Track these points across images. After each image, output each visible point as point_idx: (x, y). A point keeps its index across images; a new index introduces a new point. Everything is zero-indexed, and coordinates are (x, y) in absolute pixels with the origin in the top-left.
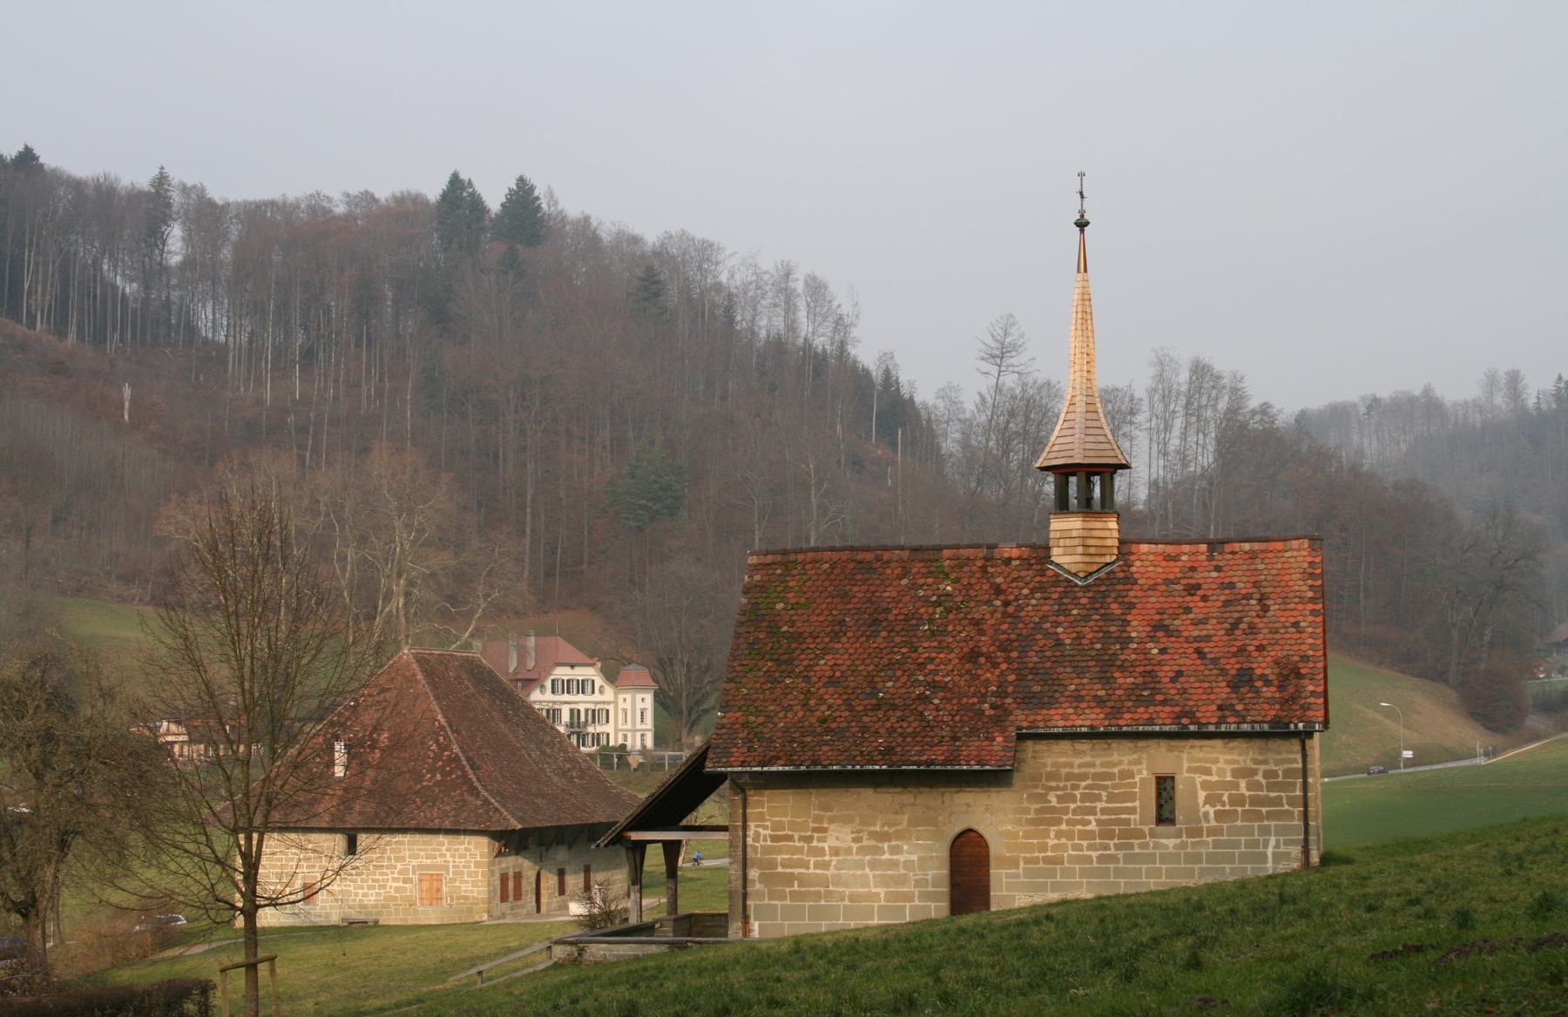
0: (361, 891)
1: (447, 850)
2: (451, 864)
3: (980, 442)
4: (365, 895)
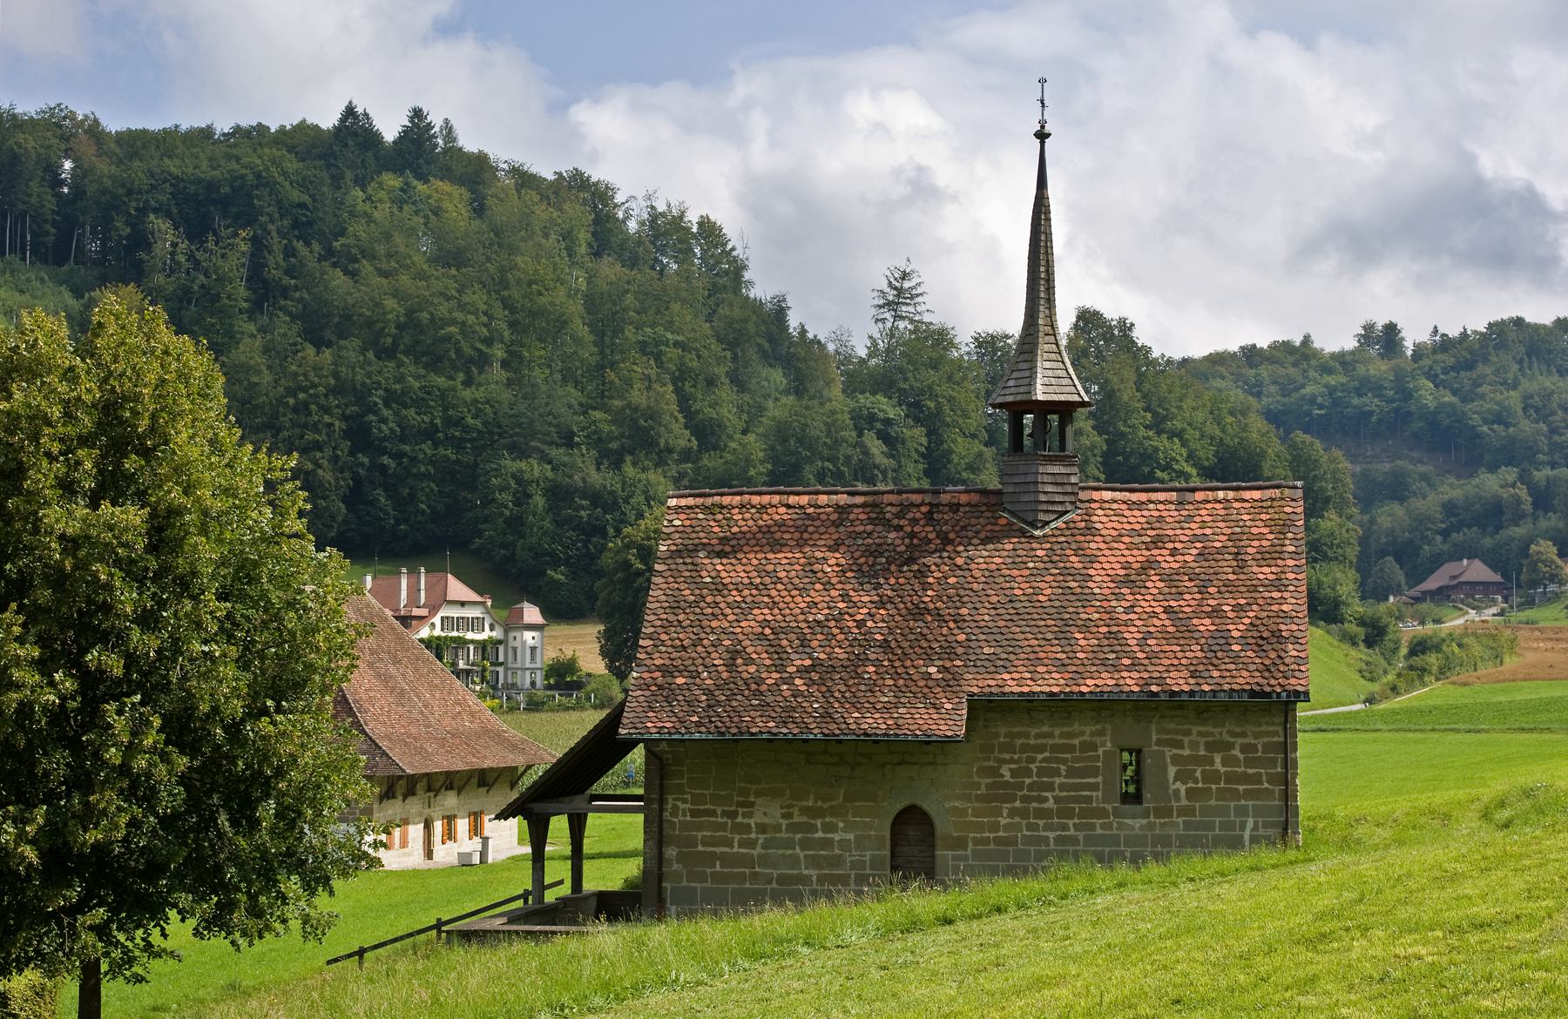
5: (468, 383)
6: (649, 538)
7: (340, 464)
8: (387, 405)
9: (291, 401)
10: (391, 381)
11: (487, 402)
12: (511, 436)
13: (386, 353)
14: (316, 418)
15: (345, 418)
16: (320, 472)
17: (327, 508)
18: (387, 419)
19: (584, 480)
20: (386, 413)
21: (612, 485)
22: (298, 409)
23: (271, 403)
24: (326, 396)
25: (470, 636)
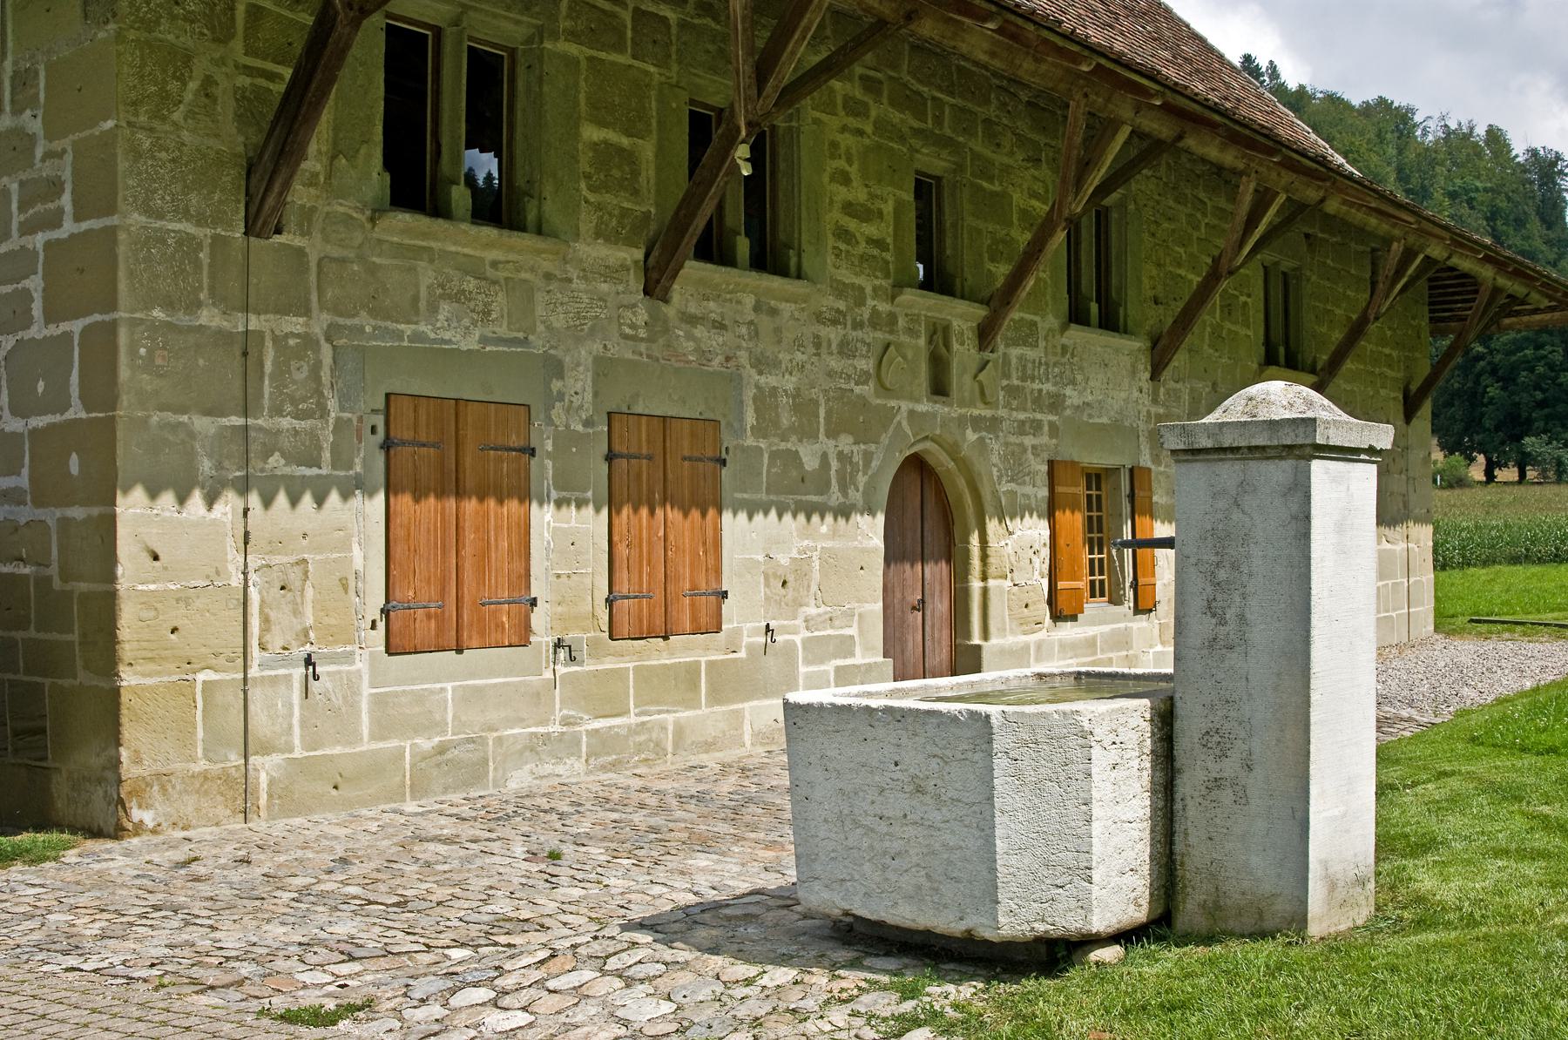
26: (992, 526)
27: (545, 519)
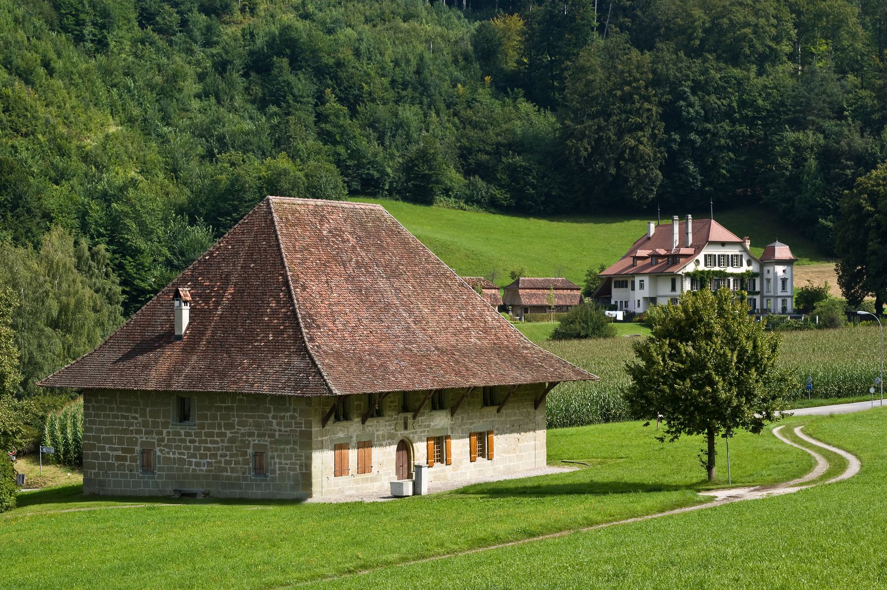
0: (194, 460)
1: (274, 417)
2: (277, 466)
3: (411, 78)
4: (198, 464)
5: (760, 74)
6: (878, 185)
7: (658, 140)
8: (694, 93)
9: (619, 93)
10: (697, 74)
11: (775, 88)
12: (794, 113)
13: (694, 53)
14: (638, 105)
15: (660, 104)
16: (641, 147)
17: (647, 175)
18: (694, 103)
19: (849, 145)
20: (692, 99)
21: (872, 148)
22: (626, 99)
23: (604, 95)
24: (646, 88)
25: (730, 270)
26: (414, 445)
27: (350, 451)
